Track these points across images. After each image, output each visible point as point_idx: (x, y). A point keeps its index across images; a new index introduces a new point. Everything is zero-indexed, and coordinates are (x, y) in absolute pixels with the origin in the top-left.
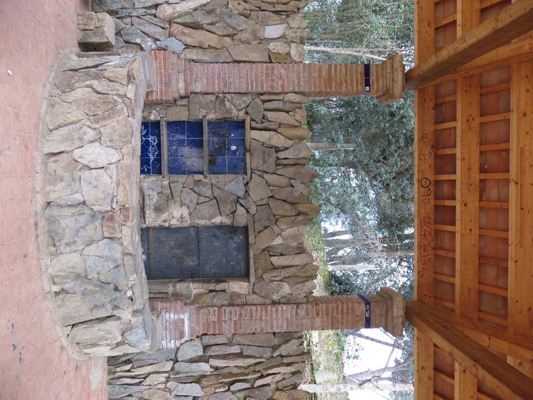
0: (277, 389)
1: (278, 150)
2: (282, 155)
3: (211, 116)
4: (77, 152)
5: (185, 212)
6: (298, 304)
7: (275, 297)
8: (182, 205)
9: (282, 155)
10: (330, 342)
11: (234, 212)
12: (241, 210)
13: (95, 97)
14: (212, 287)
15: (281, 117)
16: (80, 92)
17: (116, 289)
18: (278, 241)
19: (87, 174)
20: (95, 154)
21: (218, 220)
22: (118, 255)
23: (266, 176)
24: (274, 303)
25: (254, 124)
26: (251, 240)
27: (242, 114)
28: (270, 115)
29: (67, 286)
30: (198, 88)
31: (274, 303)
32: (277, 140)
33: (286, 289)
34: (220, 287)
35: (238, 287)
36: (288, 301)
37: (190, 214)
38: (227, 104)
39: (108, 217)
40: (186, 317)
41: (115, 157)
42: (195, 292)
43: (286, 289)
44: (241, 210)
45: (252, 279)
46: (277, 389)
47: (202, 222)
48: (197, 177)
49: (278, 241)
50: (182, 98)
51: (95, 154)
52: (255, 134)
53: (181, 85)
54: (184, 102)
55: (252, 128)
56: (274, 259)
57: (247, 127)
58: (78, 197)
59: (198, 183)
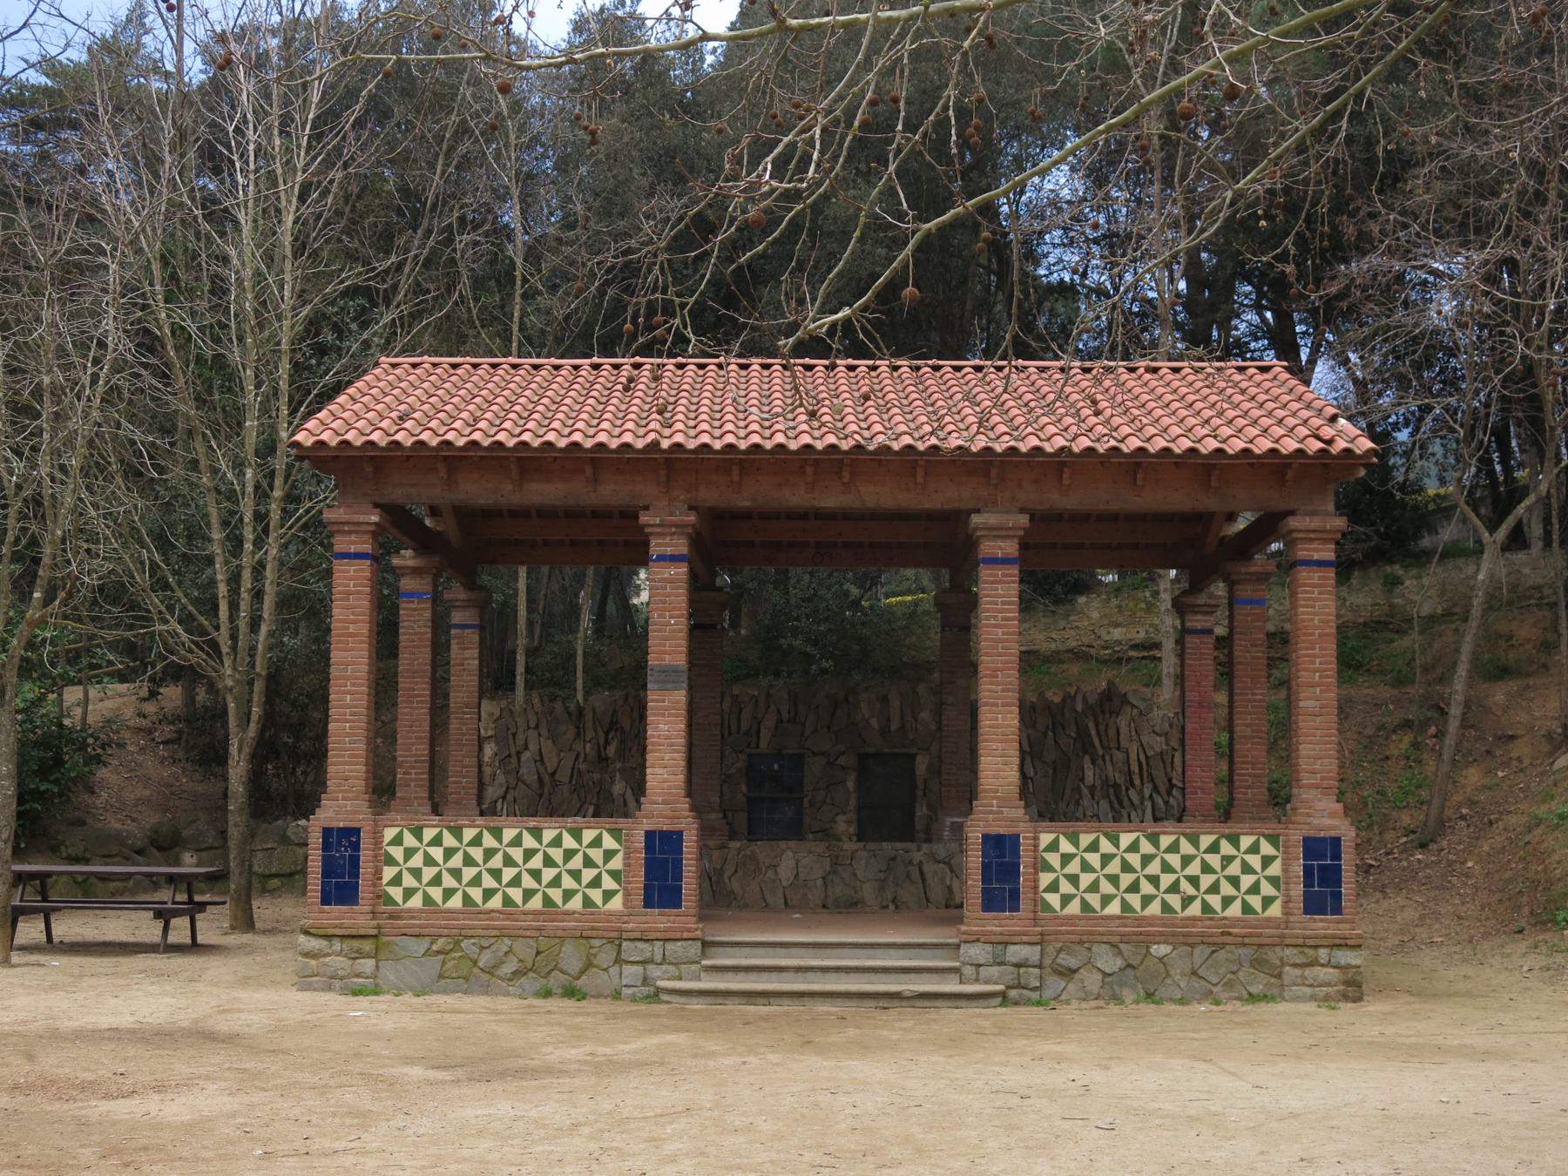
0: (1034, 727)
1: (780, 721)
2: (785, 716)
3: (744, 788)
4: (785, 883)
5: (841, 818)
6: (942, 703)
7: (933, 727)
8: (833, 821)
9: (785, 716)
10: (1131, 605)
11: (843, 768)
12: (842, 761)
13: (740, 873)
14: (920, 793)
15: (746, 716)
16: (735, 885)
17: (893, 859)
18: (874, 722)
19: (802, 876)
20: (786, 871)
21: (850, 784)
22: (865, 854)
23: (807, 733)
24: (939, 729)
25: (753, 745)
26: (872, 750)
27: (743, 757)
28: (744, 728)
29: (890, 897)
30: (716, 799)
31: (939, 729)
32: (770, 721)
33: (925, 715)
34: (920, 783)
35: (922, 765)
36: (938, 713)
37: (844, 813)
38: (732, 771)
39: (835, 862)
40: (949, 820)
41: (790, 854)
42: (925, 810)
43: (925, 715)
44: (842, 761)
45: (914, 750)
46: (1034, 727)
47: (853, 802)
48: (806, 804)
49: (874, 722)
50: (725, 817)
51: (786, 871)
52: (763, 745)
53: (714, 816)
54: (730, 815)
55: (757, 746)
56: (893, 728)
57: (754, 751)
58: (819, 882)
59: (811, 804)
